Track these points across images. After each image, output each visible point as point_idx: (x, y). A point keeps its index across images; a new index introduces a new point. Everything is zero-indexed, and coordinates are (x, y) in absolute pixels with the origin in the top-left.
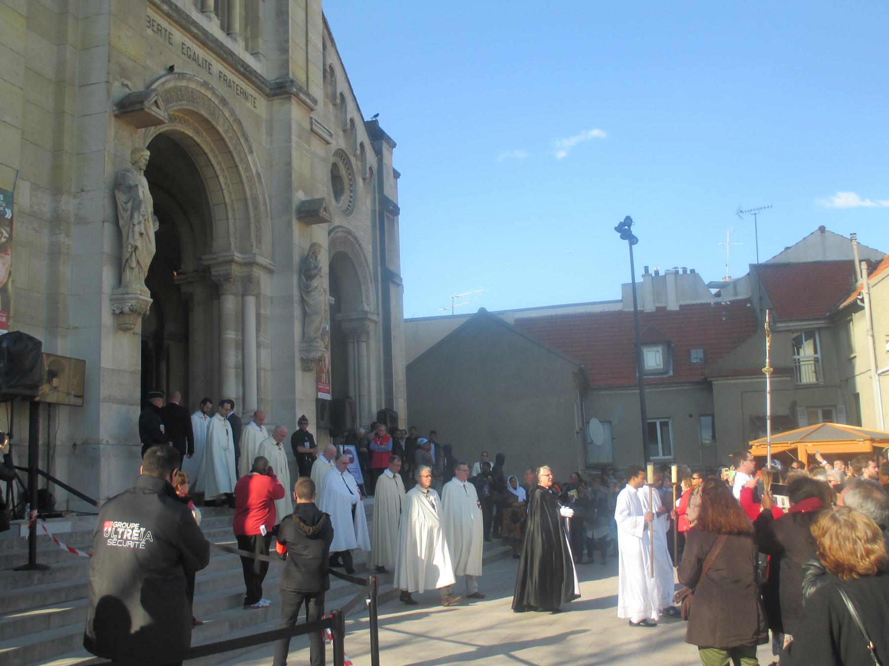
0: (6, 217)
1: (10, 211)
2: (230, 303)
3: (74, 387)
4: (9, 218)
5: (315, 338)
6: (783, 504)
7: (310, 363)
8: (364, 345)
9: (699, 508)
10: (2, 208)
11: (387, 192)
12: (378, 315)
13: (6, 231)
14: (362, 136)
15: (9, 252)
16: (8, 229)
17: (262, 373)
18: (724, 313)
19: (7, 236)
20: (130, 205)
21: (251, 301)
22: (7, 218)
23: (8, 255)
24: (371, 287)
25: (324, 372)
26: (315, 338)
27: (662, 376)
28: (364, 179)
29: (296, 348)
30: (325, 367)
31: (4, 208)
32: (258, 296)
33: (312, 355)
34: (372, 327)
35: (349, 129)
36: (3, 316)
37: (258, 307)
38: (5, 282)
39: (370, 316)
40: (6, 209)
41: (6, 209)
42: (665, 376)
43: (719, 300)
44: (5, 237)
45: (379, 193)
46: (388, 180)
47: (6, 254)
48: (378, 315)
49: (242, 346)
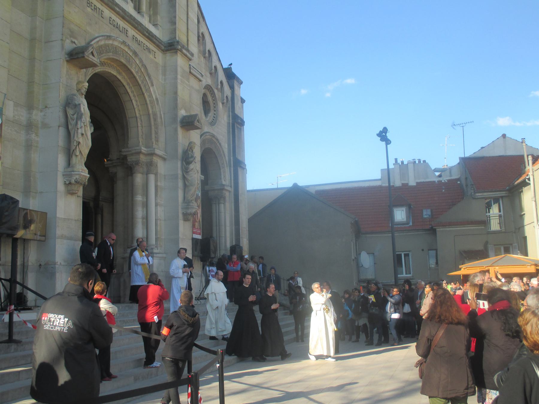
2: (139, 179)
8: (222, 206)
11: (237, 111)
12: (231, 187)
14: (221, 76)
18: (443, 187)
20: (75, 116)
21: (152, 177)
24: (227, 170)
26: (191, 201)
27: (405, 226)
28: (223, 103)
29: (179, 206)
30: (198, 219)
32: (156, 174)
33: (189, 211)
34: (227, 194)
35: (213, 72)
37: (156, 181)
39: (226, 188)
42: (407, 226)
43: (441, 179)
45: (232, 112)
46: (238, 104)
49: (146, 205)
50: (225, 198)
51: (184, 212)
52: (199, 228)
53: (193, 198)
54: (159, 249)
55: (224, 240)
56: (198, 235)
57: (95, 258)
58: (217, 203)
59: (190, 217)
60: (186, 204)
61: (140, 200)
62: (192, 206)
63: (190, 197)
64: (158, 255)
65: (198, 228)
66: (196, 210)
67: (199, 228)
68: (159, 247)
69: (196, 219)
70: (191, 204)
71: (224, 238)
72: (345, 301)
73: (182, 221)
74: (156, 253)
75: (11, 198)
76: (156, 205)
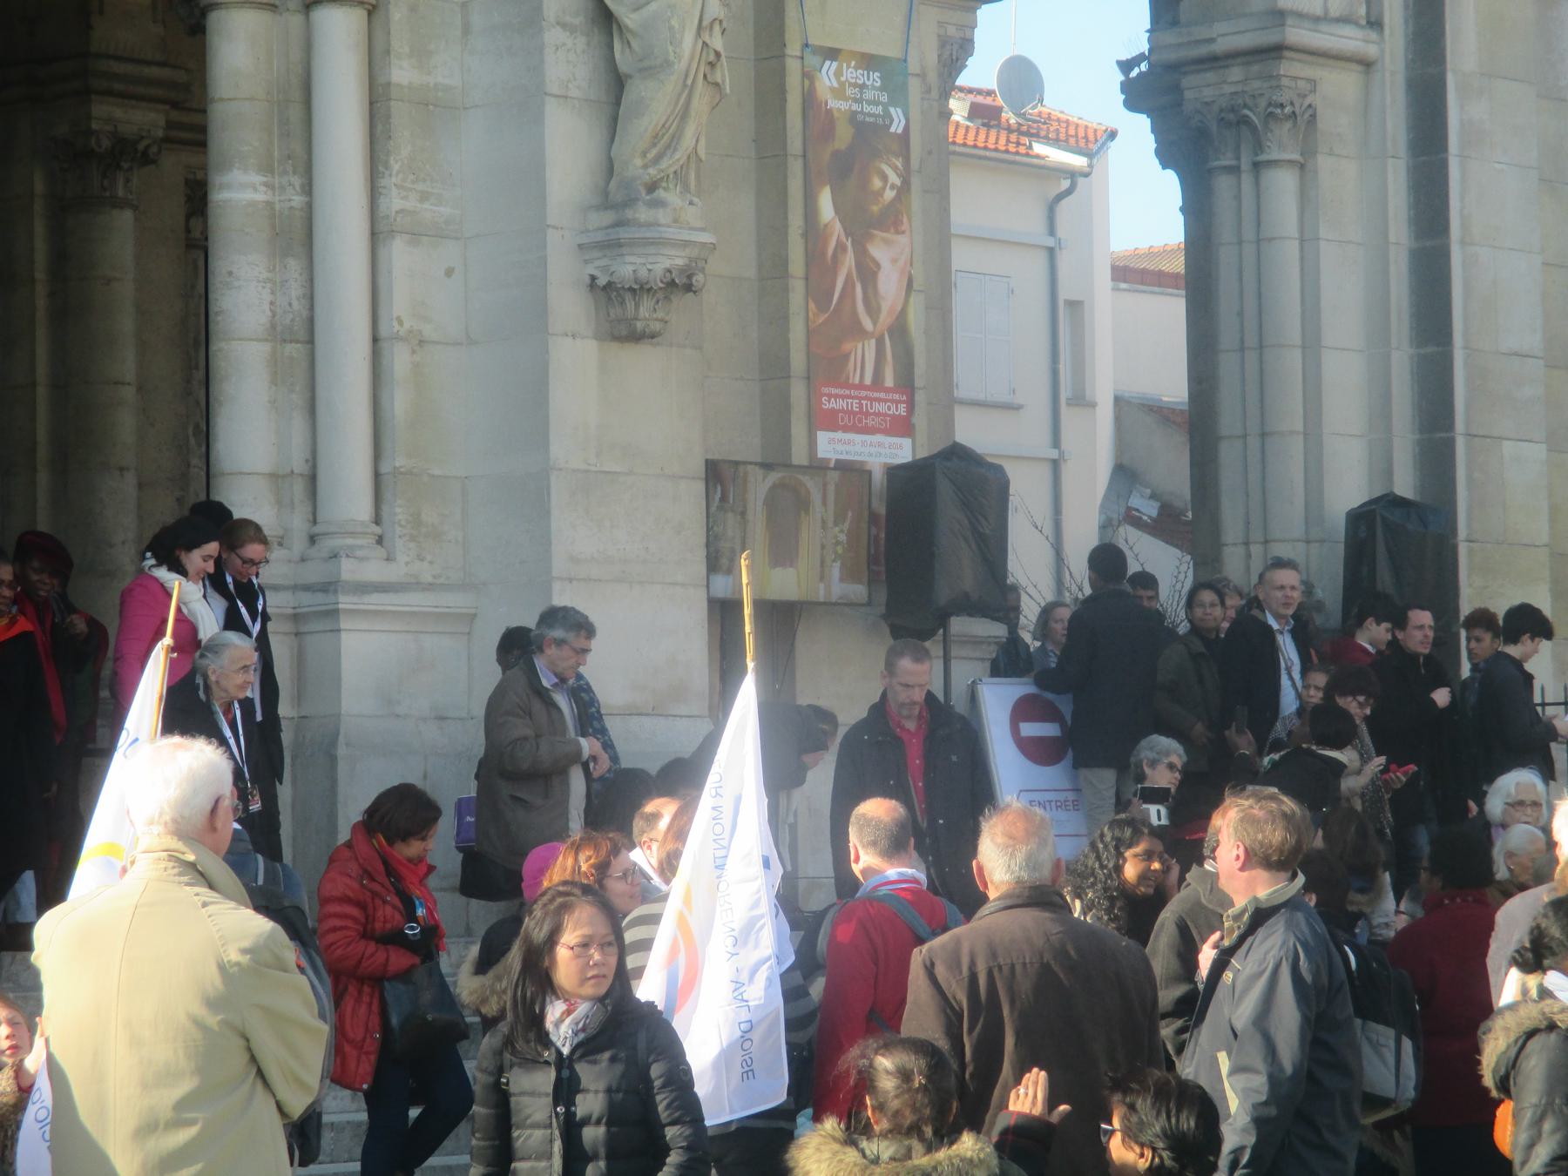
0: (892, 130)
1: (899, 111)
3: (840, 549)
4: (900, 131)
5: (652, 187)
6: (1159, 819)
7: (630, 305)
8: (1283, 183)
9: (609, 874)
10: (880, 108)
12: (1375, 23)
13: (895, 169)
15: (905, 226)
16: (899, 164)
17: (400, 360)
19: (898, 182)
22: (895, 133)
23: (903, 232)
25: (861, 333)
26: (652, 187)
29: (553, 237)
30: (873, 311)
31: (885, 106)
33: (628, 268)
34: (1338, 86)
36: (901, 402)
38: (899, 309)
40: (892, 110)
41: (892, 110)
44: (893, 187)
47: (898, 232)
48: (1375, 23)
50: (1306, 122)
51: (596, 273)
52: (889, 382)
53: (664, 164)
54: (402, 558)
55: (1298, 476)
56: (879, 438)
57: (1501, 622)
58: (1245, 164)
59: (644, 312)
60: (608, 217)
61: (252, 204)
62: (649, 225)
63: (638, 162)
64: (373, 601)
65: (877, 383)
66: (691, 260)
67: (889, 382)
68: (399, 543)
69: (855, 313)
70: (643, 214)
71: (1296, 447)
72: (1317, 905)
73: (588, 349)
74: (363, 588)
75: (1157, 23)
76: (377, 236)
